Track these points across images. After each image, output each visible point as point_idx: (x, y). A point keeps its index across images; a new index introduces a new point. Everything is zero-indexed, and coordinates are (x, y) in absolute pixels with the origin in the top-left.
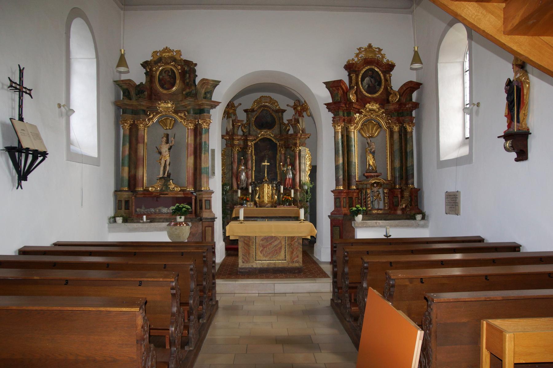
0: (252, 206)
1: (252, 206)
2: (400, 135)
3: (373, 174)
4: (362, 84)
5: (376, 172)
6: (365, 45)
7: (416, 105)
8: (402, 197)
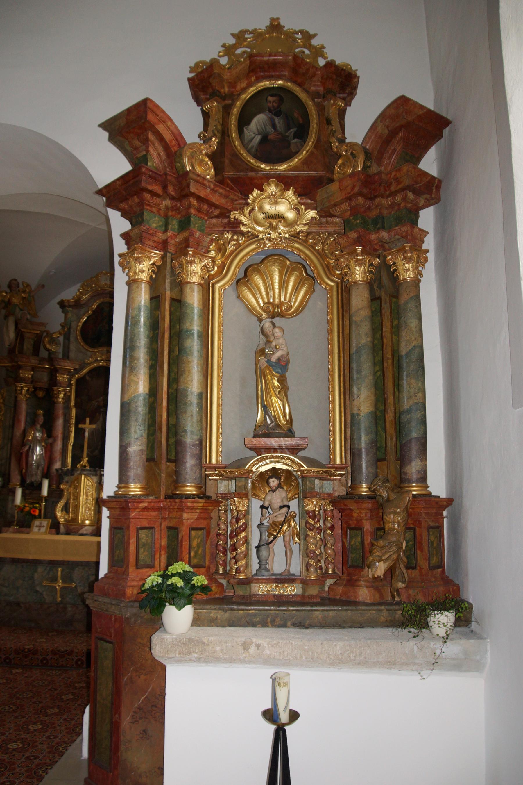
0: (43, 530)
1: (43, 530)
2: (374, 299)
3: (273, 442)
4: (241, 132)
5: (290, 433)
6: (262, 25)
7: (430, 190)
8: (380, 530)
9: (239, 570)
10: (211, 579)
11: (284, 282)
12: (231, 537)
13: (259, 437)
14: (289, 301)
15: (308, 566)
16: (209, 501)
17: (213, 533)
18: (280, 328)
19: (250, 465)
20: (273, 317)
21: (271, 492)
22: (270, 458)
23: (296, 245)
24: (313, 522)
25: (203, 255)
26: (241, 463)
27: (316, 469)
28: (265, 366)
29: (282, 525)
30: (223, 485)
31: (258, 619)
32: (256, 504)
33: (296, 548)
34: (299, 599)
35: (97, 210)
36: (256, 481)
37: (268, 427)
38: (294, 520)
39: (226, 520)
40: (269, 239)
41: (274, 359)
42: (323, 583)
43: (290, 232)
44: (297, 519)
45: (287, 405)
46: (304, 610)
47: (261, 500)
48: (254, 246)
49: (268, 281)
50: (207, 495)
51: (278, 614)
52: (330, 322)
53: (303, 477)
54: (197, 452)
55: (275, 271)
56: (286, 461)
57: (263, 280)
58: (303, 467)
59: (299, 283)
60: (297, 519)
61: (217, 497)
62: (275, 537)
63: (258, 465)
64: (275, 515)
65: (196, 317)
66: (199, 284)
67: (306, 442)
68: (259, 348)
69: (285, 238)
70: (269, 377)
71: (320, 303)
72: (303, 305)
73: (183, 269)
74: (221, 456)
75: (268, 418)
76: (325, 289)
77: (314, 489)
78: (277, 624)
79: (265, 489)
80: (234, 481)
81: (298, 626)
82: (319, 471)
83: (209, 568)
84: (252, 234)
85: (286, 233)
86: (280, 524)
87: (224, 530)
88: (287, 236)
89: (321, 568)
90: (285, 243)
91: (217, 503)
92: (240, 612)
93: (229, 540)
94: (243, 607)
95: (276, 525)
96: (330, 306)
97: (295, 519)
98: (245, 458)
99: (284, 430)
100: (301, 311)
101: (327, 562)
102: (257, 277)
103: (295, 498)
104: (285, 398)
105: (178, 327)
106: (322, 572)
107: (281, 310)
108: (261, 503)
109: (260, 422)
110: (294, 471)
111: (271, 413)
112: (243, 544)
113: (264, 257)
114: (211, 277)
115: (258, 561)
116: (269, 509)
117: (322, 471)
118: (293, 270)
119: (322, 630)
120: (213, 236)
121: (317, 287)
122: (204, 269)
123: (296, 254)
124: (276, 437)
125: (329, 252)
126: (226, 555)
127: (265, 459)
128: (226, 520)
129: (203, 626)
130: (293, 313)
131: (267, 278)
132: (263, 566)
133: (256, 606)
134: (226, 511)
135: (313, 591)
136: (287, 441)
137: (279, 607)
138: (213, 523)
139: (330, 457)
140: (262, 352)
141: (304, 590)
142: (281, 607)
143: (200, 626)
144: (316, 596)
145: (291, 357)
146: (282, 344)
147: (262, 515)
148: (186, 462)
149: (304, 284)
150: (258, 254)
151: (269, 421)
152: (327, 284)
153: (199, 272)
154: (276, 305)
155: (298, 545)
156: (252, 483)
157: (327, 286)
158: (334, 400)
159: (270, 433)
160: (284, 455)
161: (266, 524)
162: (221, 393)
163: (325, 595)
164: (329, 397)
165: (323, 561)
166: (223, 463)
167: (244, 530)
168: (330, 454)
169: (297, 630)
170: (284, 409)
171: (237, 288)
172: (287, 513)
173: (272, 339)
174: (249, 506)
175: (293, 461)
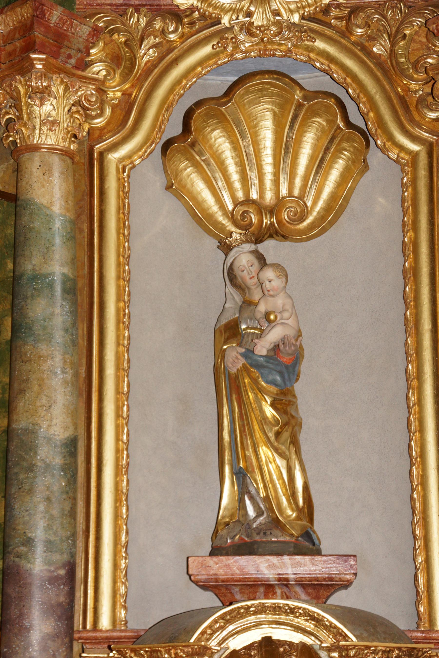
3: (264, 567)
5: (307, 544)
11: (287, 148)
13: (227, 554)
14: (301, 197)
18: (277, 267)
19: (203, 633)
20: (258, 240)
22: (255, 613)
23: (320, 44)
25: (74, 75)
27: (382, 646)
28: (239, 366)
37: (249, 526)
40: (248, 29)
41: (262, 348)
43: (304, 7)
45: (298, 467)
48: (207, 50)
49: (245, 143)
52: (411, 249)
54: (62, 599)
55: (263, 118)
56: (301, 622)
57: (232, 142)
59: (327, 149)
63: (225, 633)
65: (58, 241)
66: (65, 153)
67: (351, 567)
68: (223, 321)
69: (291, 26)
70: (251, 395)
71: (381, 200)
72: (336, 208)
73: (19, 110)
74: (126, 608)
75: (248, 502)
76: (397, 161)
82: (391, 651)
84: (203, 17)
85: (292, 12)
88: (296, 18)
90: (289, 39)
96: (410, 207)
98: (190, 614)
99: (292, 535)
100: (332, 223)
102: (217, 133)
104: (293, 450)
105: (10, 266)
107: (279, 222)
109: (227, 513)
110: (321, 648)
111: (257, 490)
113: (236, 78)
114: (95, 135)
117: (399, 649)
118: (313, 112)
120: (99, 19)
121: (375, 157)
122: (78, 112)
123: (320, 70)
124: (272, 554)
125: (408, 60)
127: (242, 616)
130: (312, 227)
131: (243, 137)
139: (418, 612)
140: (230, 331)
145: (305, 341)
146: (283, 310)
148: (28, 630)
149: (339, 151)
150: (218, 70)
151: (251, 512)
152: (402, 148)
153: (65, 122)
154: (265, 208)
157: (402, 155)
158: (423, 455)
159: (255, 542)
160: (292, 603)
162: (125, 437)
164: (410, 447)
166: (132, 625)
168: (417, 603)
170: (291, 478)
171: (164, 165)
173: (256, 296)
175: (318, 621)
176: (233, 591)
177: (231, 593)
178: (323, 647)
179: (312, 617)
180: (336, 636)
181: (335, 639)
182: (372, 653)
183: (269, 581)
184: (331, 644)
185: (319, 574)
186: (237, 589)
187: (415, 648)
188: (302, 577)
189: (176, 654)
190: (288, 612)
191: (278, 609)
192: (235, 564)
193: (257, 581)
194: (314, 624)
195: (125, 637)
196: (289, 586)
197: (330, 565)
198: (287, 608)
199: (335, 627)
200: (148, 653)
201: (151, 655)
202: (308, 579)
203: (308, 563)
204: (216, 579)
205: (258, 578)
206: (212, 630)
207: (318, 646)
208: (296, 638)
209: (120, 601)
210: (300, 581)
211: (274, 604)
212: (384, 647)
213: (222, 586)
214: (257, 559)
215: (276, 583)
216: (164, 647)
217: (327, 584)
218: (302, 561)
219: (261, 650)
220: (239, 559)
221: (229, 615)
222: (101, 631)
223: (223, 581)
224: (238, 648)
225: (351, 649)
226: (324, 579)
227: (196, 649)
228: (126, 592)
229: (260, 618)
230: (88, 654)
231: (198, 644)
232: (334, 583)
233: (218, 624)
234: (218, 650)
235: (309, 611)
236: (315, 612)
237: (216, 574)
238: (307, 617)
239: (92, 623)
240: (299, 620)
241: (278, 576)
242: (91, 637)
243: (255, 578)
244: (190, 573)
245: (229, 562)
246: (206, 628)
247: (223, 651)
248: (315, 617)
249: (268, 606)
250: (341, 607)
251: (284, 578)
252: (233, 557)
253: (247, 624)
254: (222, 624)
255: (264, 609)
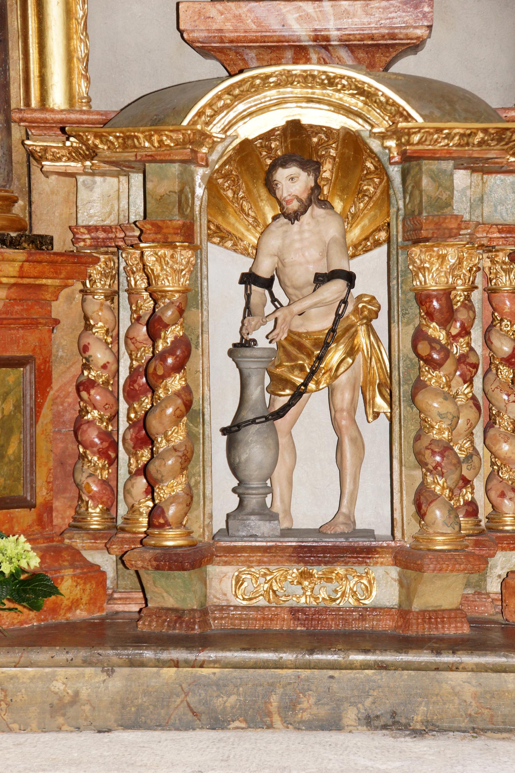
9: (163, 513)
10: (54, 550)
12: (132, 396)
15: (422, 501)
16: (45, 257)
17: (64, 376)
19: (199, 114)
21: (283, 220)
22: (277, 85)
24: (442, 336)
26: (160, 108)
27: (460, 127)
29: (325, 346)
30: (97, 192)
31: (233, 699)
32: (223, 267)
33: (375, 434)
34: (386, 625)
35: (131, 104)
36: (226, 177)
38: (370, 330)
39: (112, 331)
42: (480, 564)
44: (380, 324)
46: (407, 667)
47: (245, 252)
50: (36, 231)
51: (307, 679)
53: (409, 160)
56: (348, 99)
58: (408, 118)
60: (380, 324)
61: (75, 241)
62: (298, 394)
63: (232, 115)
64: (297, 308)
77: (449, 204)
78: (306, 716)
79: (259, 210)
80: (137, 179)
81: (385, 727)
83: (48, 508)
86: (316, 344)
87: (104, 367)
89: (472, 510)
91: (77, 263)
92: (163, 674)
93: (123, 406)
94: (176, 654)
95: (300, 347)
97: (374, 323)
101: (496, 487)
103: (377, 244)
106: (478, 524)
108: (245, 265)
110: (372, 135)
112: (178, 418)
115: (235, 483)
116: (276, 288)
117: (485, 131)
119: (479, 743)
126: (113, 461)
127: (257, 90)
128: (112, 331)
129: (24, 729)
132: (252, 502)
133: (224, 648)
134: (112, 296)
135: (442, 592)
136: (347, 14)
137: (311, 652)
138: (63, 342)
141: (407, 589)
142: (322, 652)
143: (11, 730)
144: (455, 614)
147: (248, 310)
155: (383, 421)
156: (211, 185)
161: (263, 343)
163: (488, 610)
165: (479, 484)
166: (97, 105)
167: (179, 367)
169: (382, 740)
172: (345, 301)
174: (197, 272)
176: (246, 57)
177: (244, 60)
178: (375, 133)
179: (361, 91)
180: (394, 116)
181: (392, 122)
182: (444, 138)
183: (299, 41)
184: (386, 129)
185: (376, 29)
186: (252, 54)
187: (507, 129)
188: (350, 35)
189: (161, 142)
190: (325, 84)
191: (310, 79)
192: (249, 14)
193: (283, 42)
194: (362, 101)
195: (87, 122)
196: (330, 48)
197: (393, 15)
198: (323, 77)
199: (394, 104)
200: (120, 140)
201: (125, 142)
202: (358, 37)
203: (360, 12)
204: (221, 37)
205: (284, 36)
206: (213, 110)
207: (368, 133)
208: (337, 121)
209: (78, 67)
210: (346, 41)
211: (305, 71)
212: (463, 128)
213: (230, 49)
214: (282, 7)
215: (311, 43)
216: (143, 132)
217: (386, 45)
218: (351, 9)
219: (285, 141)
220: (255, 7)
221: (239, 87)
222: (52, 111)
223: (232, 41)
224: (251, 137)
225: (415, 133)
226: (383, 37)
227: (189, 135)
228: (87, 55)
229: (283, 93)
230: (35, 141)
231: (192, 127)
232: (397, 41)
233: (222, 102)
234: (222, 138)
235: (356, 81)
236: (364, 83)
237: (220, 31)
238: (353, 90)
239: (38, 99)
240: (341, 95)
241: (313, 34)
242: (37, 118)
243: (279, 36)
244: (182, 27)
245: (241, 11)
246: (204, 107)
247: (228, 141)
248: (364, 90)
249: (296, 75)
250: (404, 76)
251: (322, 36)
252: (247, 3)
253: (265, 102)
254: (229, 101)
255: (290, 79)
